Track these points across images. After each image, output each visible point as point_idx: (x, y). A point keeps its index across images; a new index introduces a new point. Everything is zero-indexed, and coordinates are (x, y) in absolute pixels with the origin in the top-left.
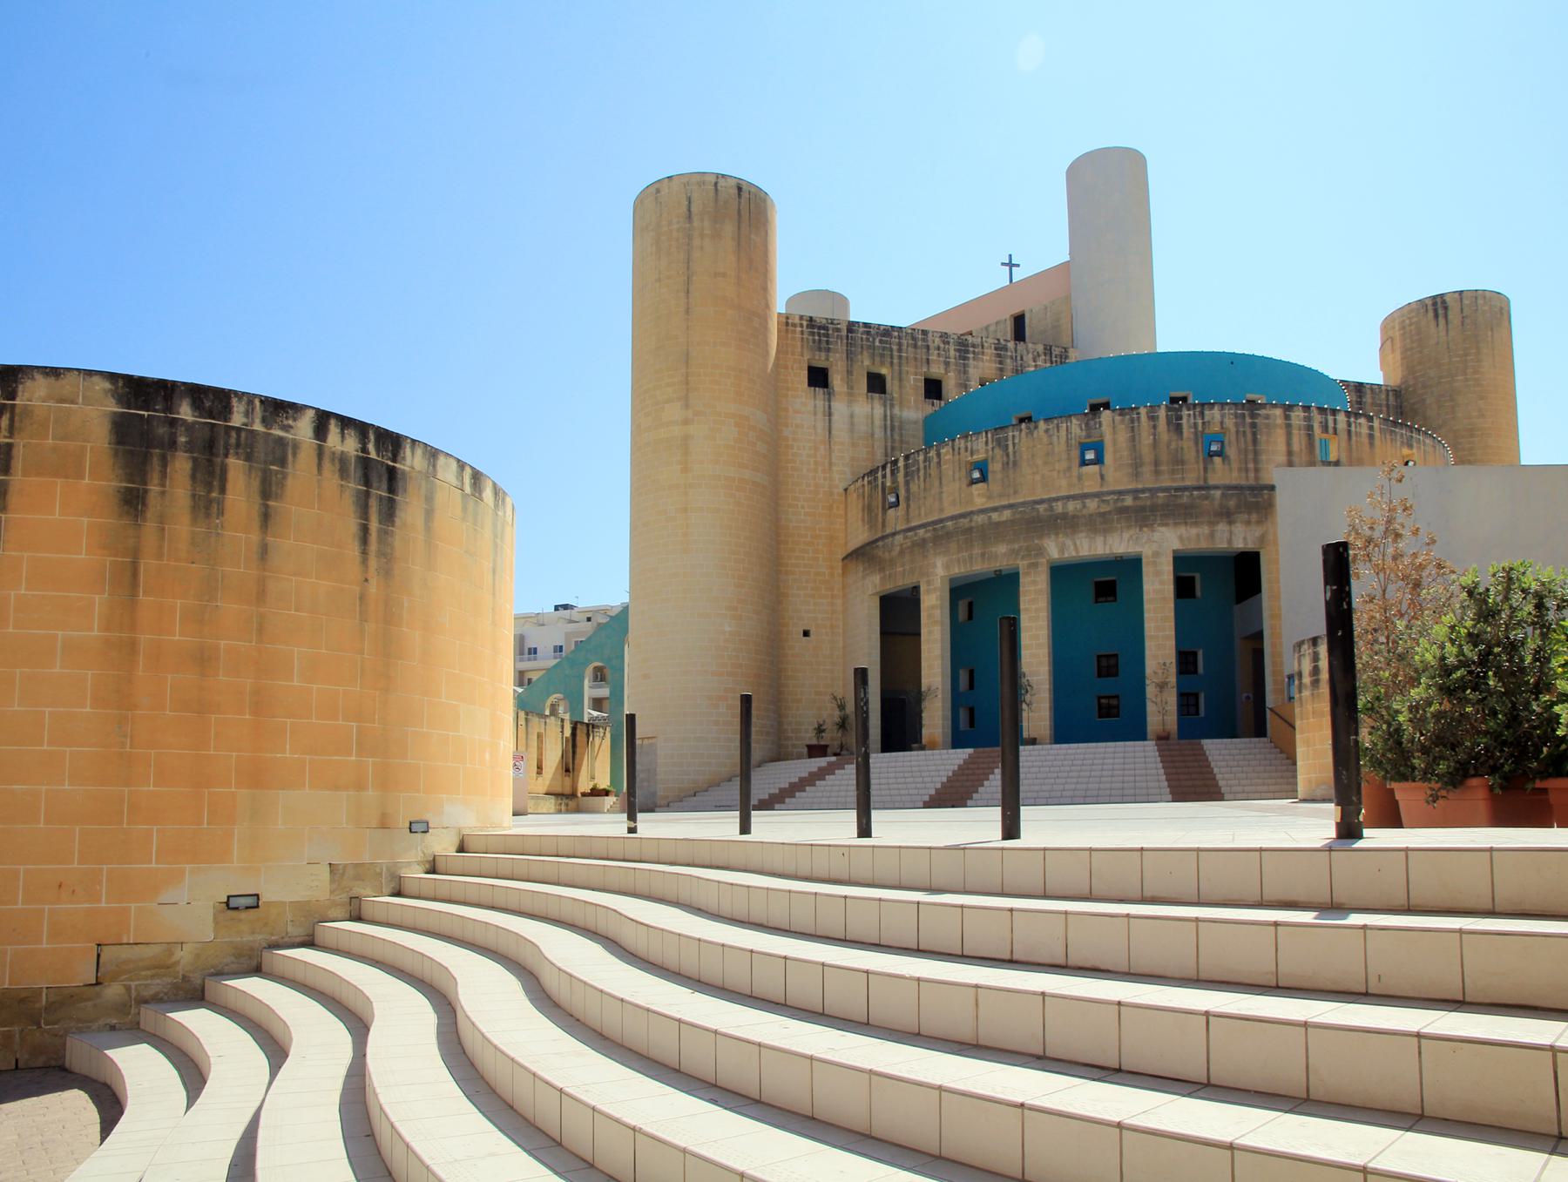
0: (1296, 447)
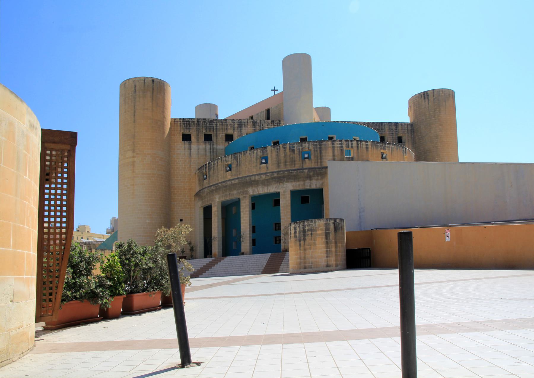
0: (336, 153)
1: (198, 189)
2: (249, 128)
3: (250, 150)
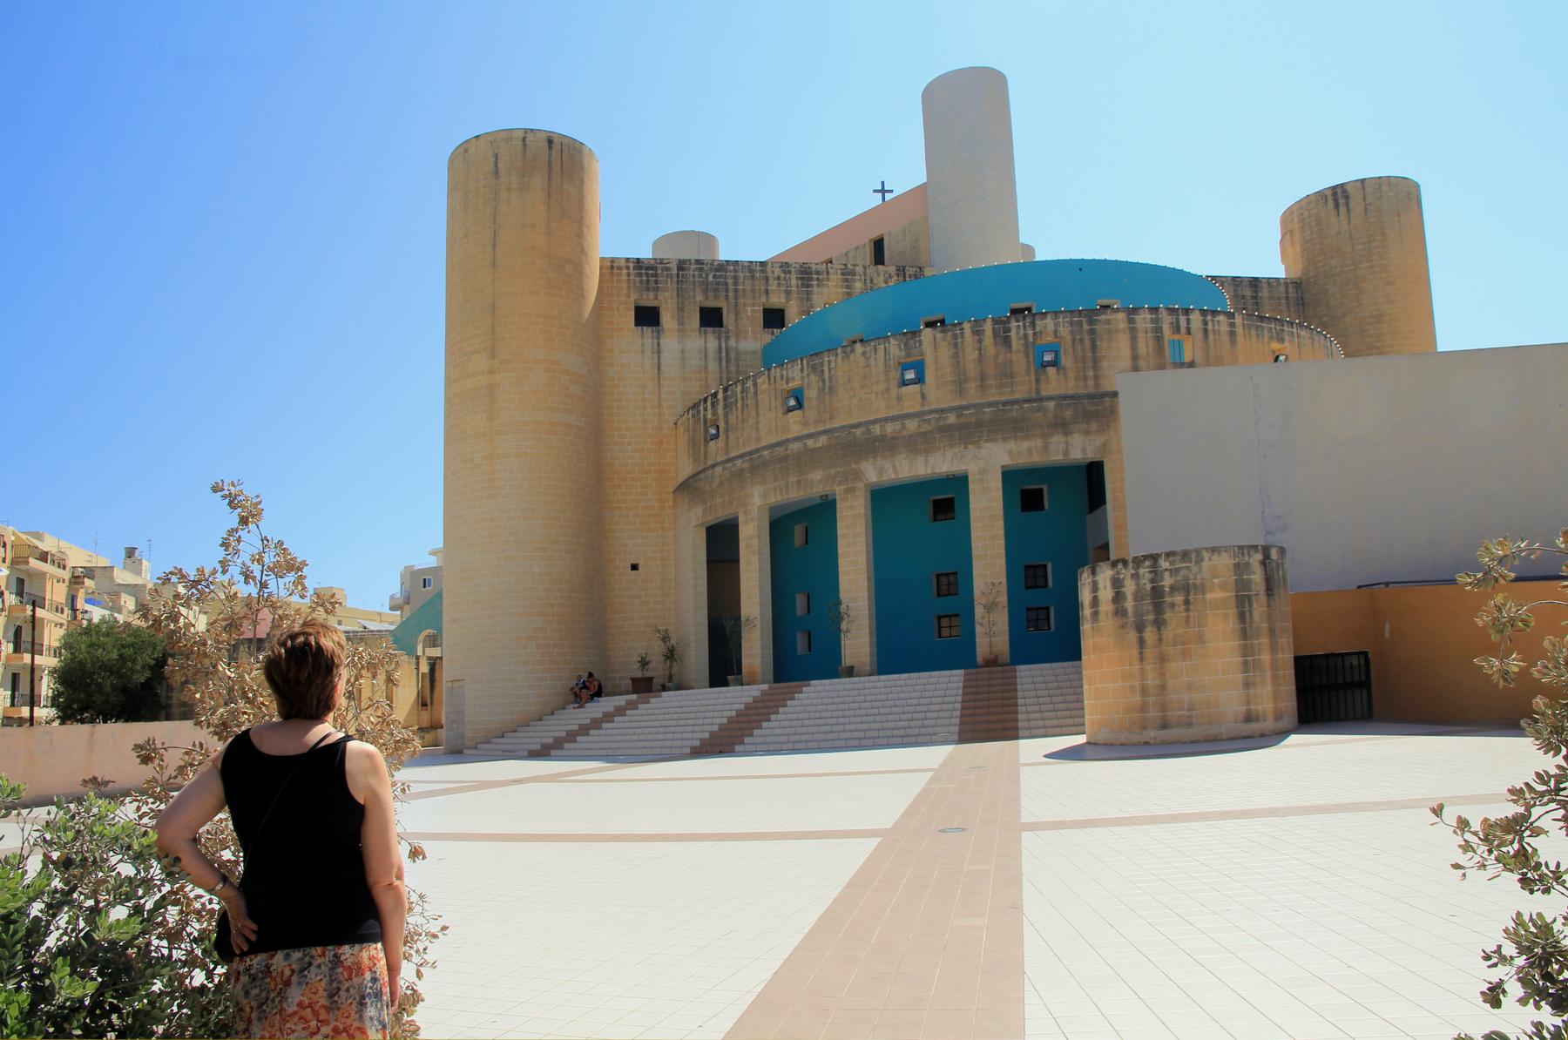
0: (1142, 350)
1: (686, 469)
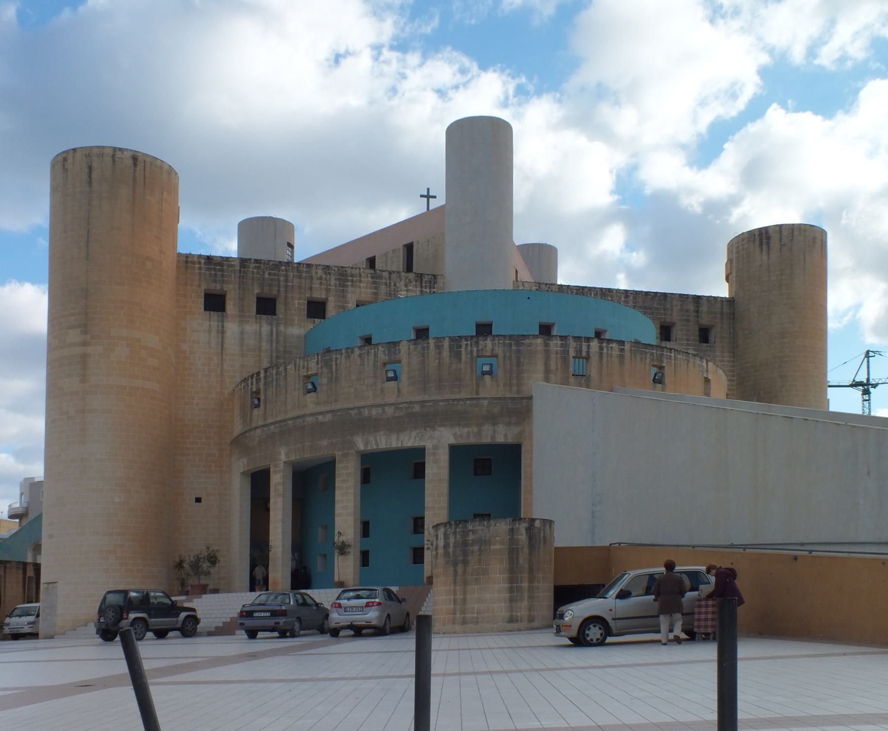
0: (553, 366)
2: (362, 290)
3: (360, 347)
